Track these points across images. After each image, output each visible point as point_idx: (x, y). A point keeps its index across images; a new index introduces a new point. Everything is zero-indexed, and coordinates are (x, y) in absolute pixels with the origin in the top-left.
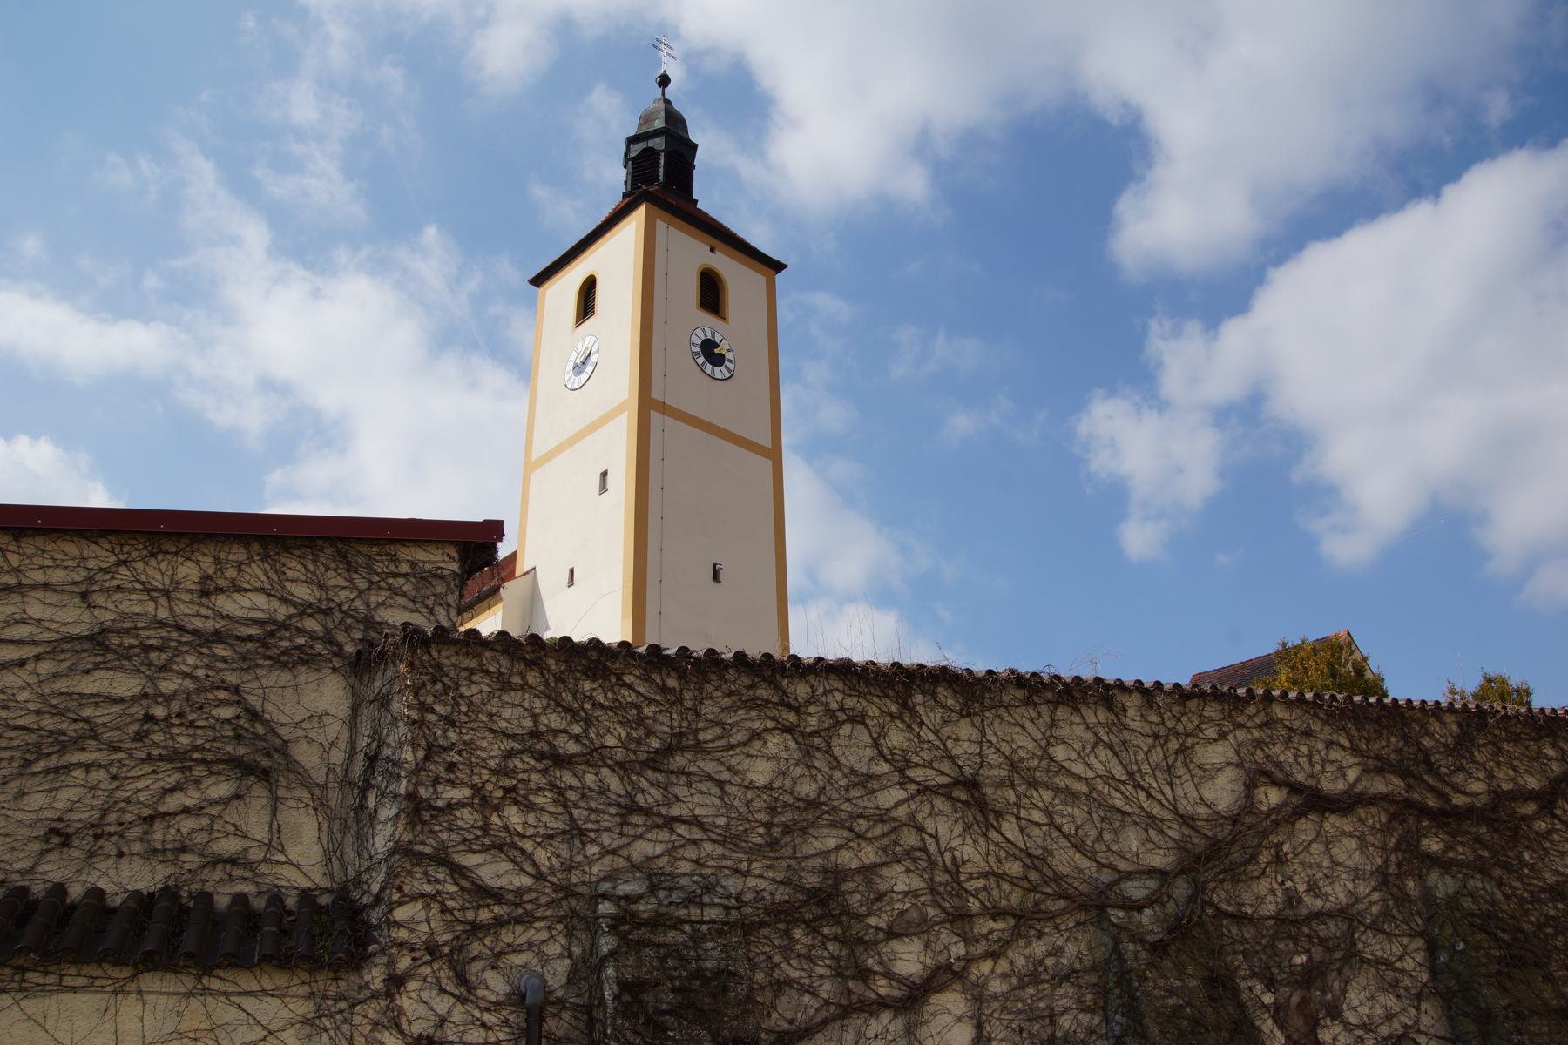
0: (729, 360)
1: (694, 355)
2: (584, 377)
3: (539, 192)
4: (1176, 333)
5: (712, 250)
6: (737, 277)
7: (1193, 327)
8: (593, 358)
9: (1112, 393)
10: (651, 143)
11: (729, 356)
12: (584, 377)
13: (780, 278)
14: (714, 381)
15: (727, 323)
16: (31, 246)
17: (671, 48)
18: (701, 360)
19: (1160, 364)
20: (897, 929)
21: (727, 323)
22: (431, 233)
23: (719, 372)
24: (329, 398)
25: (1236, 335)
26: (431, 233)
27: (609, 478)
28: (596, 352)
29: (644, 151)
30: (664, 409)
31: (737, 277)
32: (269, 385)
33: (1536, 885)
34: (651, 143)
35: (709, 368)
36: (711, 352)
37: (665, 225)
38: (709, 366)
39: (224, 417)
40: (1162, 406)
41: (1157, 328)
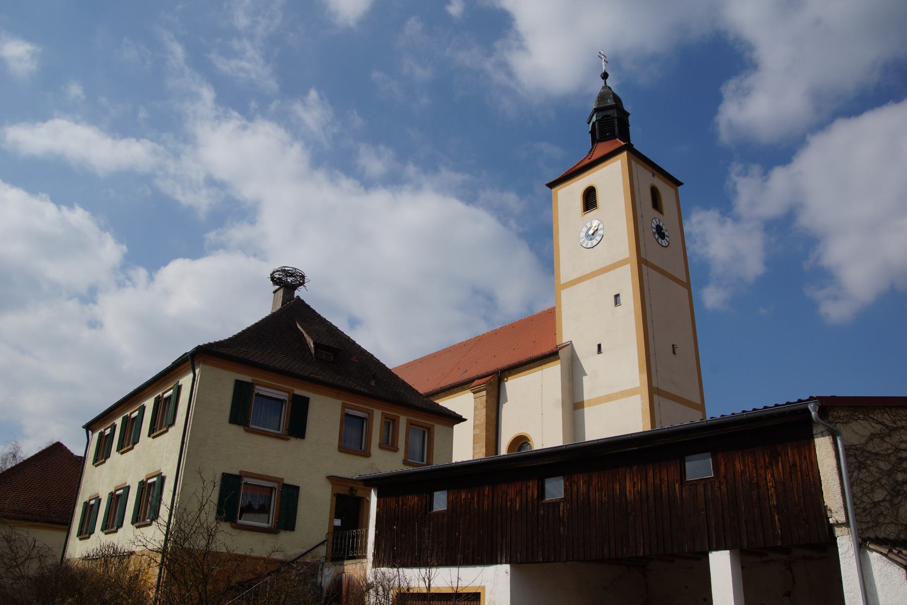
0: (667, 236)
1: (654, 233)
2: (595, 242)
3: (376, 75)
4: (745, 173)
5: (653, 175)
6: (665, 190)
7: (756, 169)
8: (600, 232)
9: (706, 207)
10: (608, 113)
11: (666, 233)
12: (595, 242)
13: (680, 188)
14: (663, 248)
15: (663, 215)
16: (75, 90)
17: (599, 56)
18: (657, 236)
19: (735, 192)
20: (119, 526)
21: (663, 215)
22: (313, 94)
23: (664, 243)
24: (248, 192)
25: (780, 178)
26: (313, 94)
27: (622, 299)
28: (601, 229)
29: (604, 116)
30: (647, 263)
31: (665, 190)
32: (212, 182)
33: (564, 506)
34: (608, 113)
35: (660, 240)
36: (659, 231)
37: (635, 163)
38: (660, 239)
39: (185, 198)
40: (737, 219)
41: (736, 168)
